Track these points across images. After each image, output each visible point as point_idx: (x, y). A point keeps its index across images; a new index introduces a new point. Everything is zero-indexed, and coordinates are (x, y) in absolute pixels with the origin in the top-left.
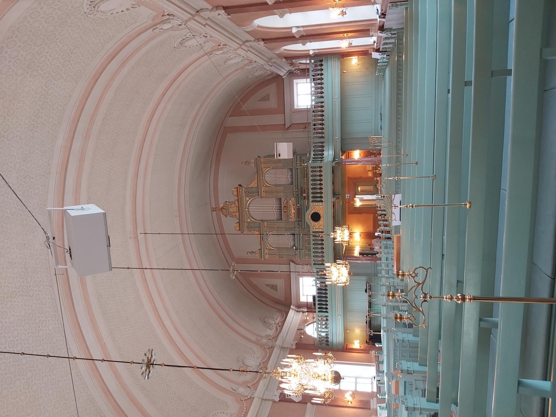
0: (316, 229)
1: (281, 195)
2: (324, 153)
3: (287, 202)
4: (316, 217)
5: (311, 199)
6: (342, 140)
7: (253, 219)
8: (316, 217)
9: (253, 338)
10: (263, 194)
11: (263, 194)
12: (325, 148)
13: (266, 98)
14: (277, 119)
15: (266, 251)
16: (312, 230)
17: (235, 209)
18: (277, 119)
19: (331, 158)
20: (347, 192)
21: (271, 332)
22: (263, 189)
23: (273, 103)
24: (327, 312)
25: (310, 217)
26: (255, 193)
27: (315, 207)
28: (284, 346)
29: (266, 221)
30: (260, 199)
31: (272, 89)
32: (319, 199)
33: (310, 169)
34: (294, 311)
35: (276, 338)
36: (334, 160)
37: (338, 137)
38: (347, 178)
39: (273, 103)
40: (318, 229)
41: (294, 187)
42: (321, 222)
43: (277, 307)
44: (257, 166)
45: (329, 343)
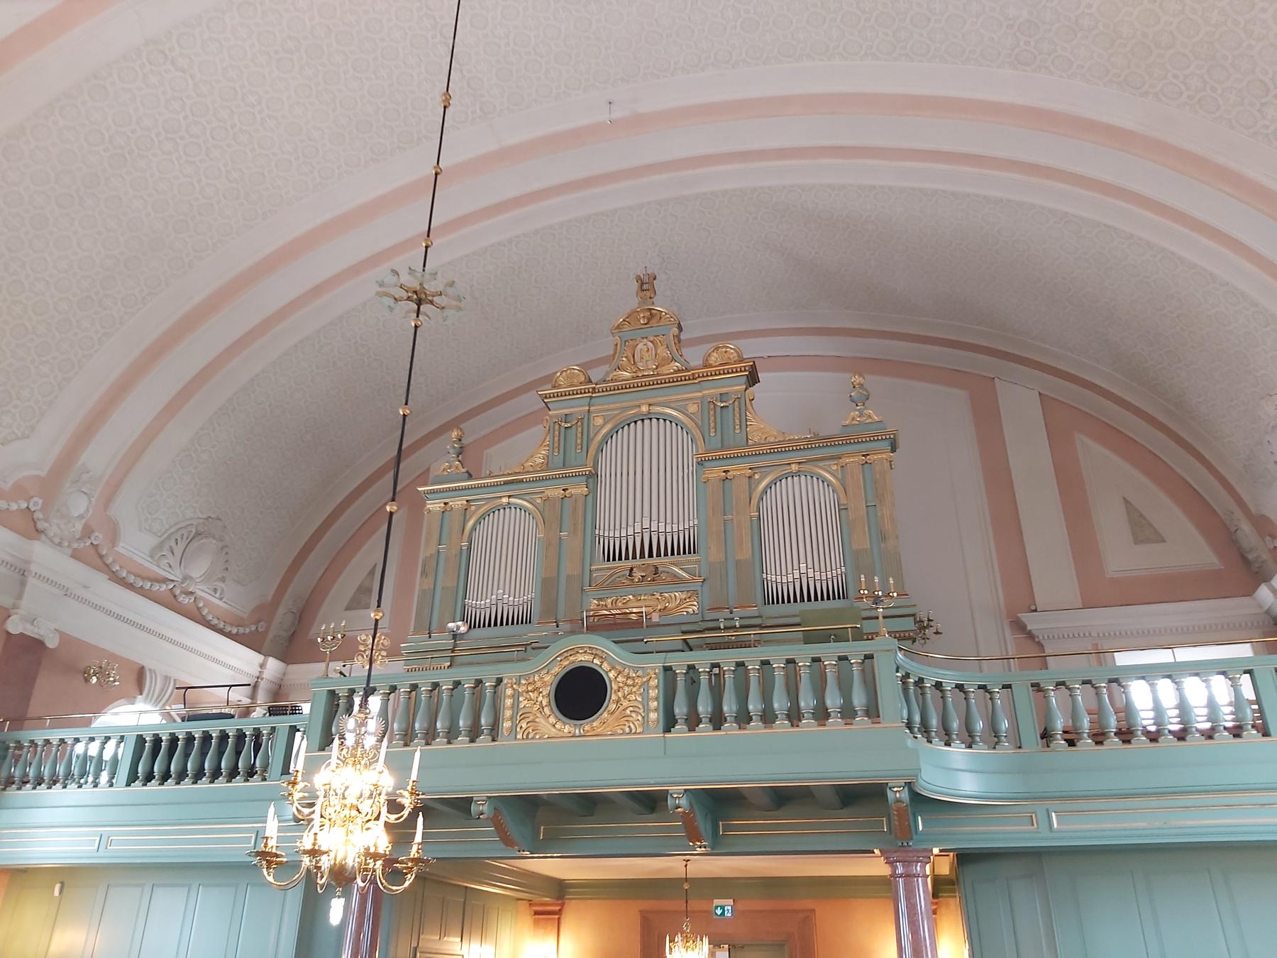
0: (517, 695)
1: (711, 552)
2: (957, 750)
3: (677, 581)
4: (580, 694)
5: (680, 662)
6: (1034, 858)
7: (605, 441)
8: (580, 694)
9: (98, 458)
10: (715, 472)
11: (715, 472)
12: (981, 750)
13: (1143, 530)
14: (1053, 576)
15: (458, 503)
16: (509, 673)
17: (648, 366)
18: (1053, 576)
19: (933, 782)
20: (741, 906)
21: (135, 546)
22: (739, 469)
23: (1122, 557)
24: (132, 778)
25: (583, 659)
26: (723, 439)
27: (633, 684)
28: (31, 581)
29: (593, 492)
30: (691, 461)
31: (1189, 550)
32: (680, 709)
33: (855, 650)
34: (255, 670)
35: (97, 558)
36: (920, 801)
37: (1060, 828)
38: (808, 904)
39: (1122, 557)
40: (515, 706)
41: (753, 611)
42: (553, 726)
43: (281, 610)
44: (849, 439)
45: (12, 792)
